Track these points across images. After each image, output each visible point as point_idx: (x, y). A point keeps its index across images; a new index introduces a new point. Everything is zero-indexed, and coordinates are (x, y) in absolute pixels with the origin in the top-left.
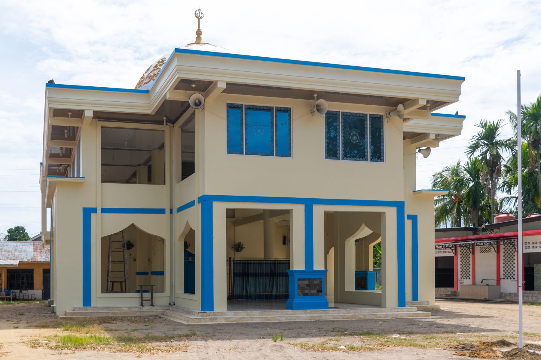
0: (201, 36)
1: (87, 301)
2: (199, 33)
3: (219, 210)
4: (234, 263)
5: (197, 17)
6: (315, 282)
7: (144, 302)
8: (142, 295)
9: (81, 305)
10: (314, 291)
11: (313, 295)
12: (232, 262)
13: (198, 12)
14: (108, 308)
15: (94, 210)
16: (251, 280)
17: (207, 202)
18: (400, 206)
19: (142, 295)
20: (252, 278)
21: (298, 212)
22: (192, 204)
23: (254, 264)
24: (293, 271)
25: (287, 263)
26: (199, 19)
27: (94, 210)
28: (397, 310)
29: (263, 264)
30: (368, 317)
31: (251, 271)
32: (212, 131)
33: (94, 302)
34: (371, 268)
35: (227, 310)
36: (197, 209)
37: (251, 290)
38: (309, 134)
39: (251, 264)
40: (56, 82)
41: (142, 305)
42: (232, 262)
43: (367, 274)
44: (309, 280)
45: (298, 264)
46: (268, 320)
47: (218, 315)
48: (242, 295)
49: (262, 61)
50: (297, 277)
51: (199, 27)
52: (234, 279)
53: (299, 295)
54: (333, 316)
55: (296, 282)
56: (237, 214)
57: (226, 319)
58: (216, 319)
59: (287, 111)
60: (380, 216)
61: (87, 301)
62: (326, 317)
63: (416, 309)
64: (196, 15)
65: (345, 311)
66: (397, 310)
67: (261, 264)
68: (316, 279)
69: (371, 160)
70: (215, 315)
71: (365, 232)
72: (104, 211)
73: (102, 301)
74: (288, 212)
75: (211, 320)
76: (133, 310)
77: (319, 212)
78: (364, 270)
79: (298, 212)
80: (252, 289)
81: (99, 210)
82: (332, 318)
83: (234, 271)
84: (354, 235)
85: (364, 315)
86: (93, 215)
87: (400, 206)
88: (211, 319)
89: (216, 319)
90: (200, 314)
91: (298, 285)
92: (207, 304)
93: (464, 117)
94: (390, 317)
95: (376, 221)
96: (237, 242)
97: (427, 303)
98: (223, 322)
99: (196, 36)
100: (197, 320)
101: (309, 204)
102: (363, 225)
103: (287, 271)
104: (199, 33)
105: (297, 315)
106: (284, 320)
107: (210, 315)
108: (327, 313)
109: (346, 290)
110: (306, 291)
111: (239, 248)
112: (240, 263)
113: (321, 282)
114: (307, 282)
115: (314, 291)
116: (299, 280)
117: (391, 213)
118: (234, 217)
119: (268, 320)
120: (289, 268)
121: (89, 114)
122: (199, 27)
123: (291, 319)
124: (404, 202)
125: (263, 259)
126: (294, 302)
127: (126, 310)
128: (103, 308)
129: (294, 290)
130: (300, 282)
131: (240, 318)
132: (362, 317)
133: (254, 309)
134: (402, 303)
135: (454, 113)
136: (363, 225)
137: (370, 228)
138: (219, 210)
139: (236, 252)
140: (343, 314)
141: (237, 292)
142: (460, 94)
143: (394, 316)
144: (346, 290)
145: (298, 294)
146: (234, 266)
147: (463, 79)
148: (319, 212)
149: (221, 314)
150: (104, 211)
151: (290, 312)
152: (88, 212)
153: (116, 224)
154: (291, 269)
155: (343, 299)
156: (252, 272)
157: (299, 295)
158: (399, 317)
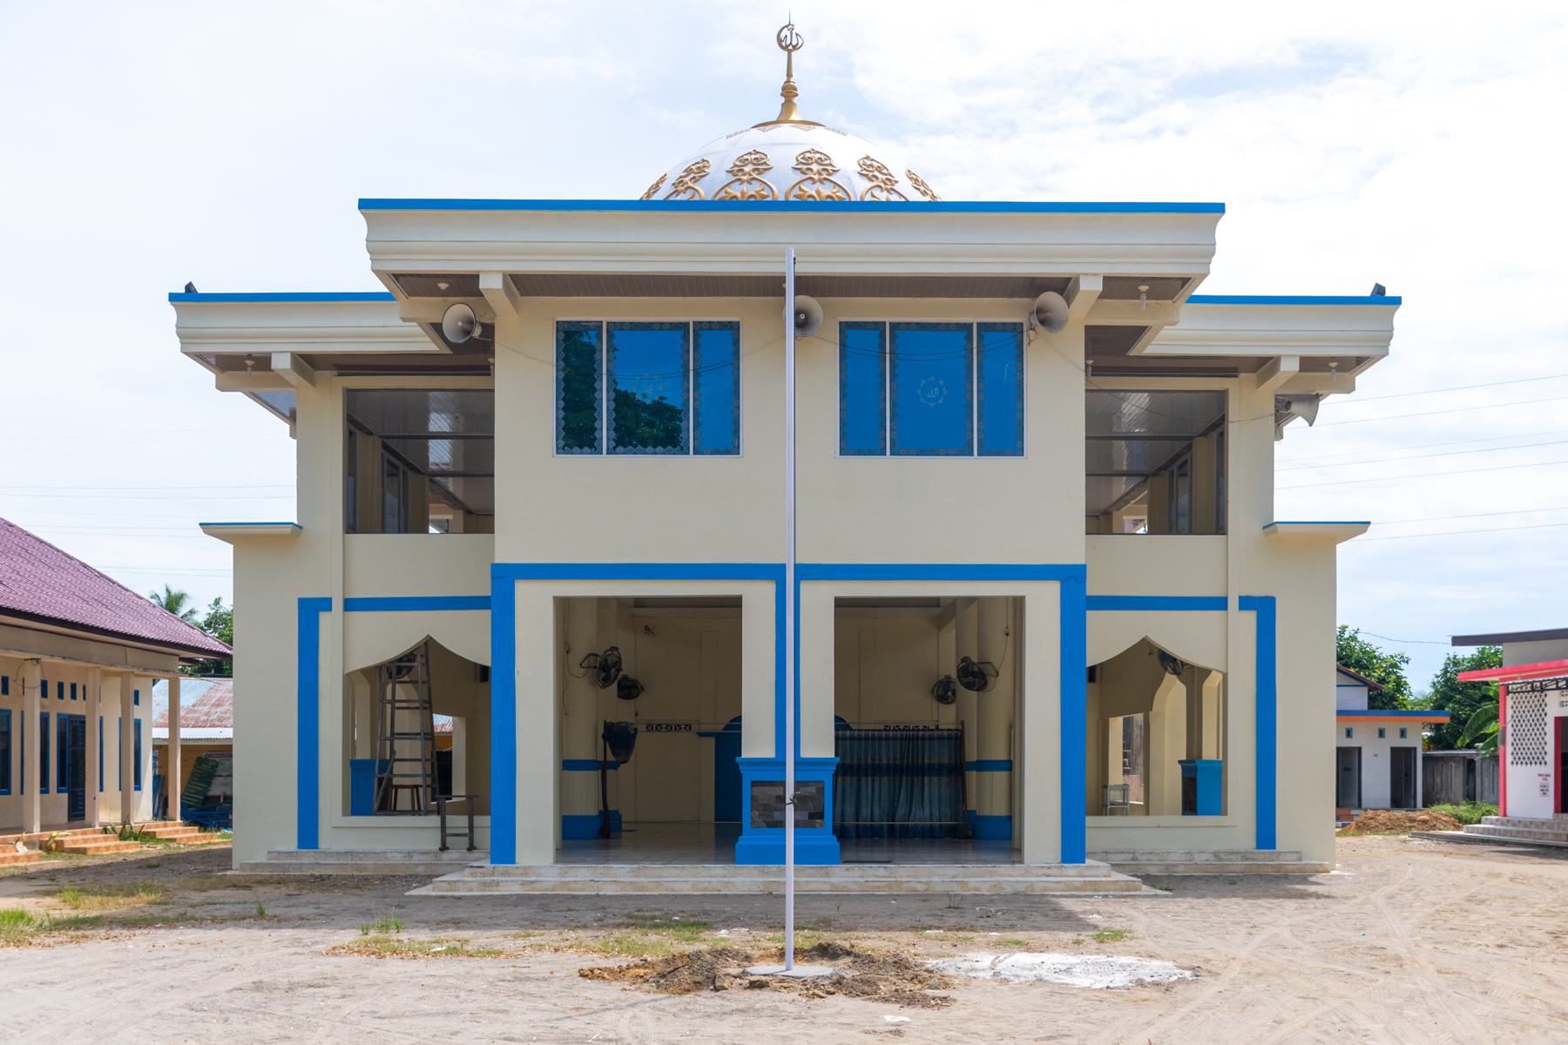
0: (795, 100)
1: (308, 834)
2: (789, 92)
3: (534, 609)
5: (785, 48)
7: (449, 839)
8: (443, 821)
9: (293, 845)
13: (786, 32)
14: (351, 853)
15: (326, 604)
19: (443, 821)
26: (790, 52)
27: (326, 604)
29: (880, 739)
32: (524, 394)
33: (329, 839)
38: (789, 392)
40: (200, 290)
41: (444, 848)
46: (643, 888)
49: (595, 213)
51: (789, 75)
53: (754, 824)
57: (523, 883)
59: (733, 328)
61: (308, 834)
62: (811, 887)
64: (780, 41)
65: (857, 873)
67: (874, 738)
69: (980, 454)
72: (350, 605)
73: (349, 837)
74: (735, 603)
76: (416, 859)
79: (757, 599)
81: (337, 605)
86: (325, 619)
88: (484, 884)
89: (497, 884)
91: (753, 798)
93: (1397, 301)
97: (1295, 856)
98: (517, 890)
99: (783, 100)
104: (789, 92)
108: (827, 875)
116: (754, 784)
121: (281, 363)
122: (789, 75)
127: (398, 859)
128: (339, 854)
130: (758, 791)
133: (924, 862)
135: (1367, 291)
142: (1213, 254)
147: (1219, 208)
148: (818, 600)
150: (350, 605)
152: (311, 610)
153: (385, 638)
157: (754, 824)
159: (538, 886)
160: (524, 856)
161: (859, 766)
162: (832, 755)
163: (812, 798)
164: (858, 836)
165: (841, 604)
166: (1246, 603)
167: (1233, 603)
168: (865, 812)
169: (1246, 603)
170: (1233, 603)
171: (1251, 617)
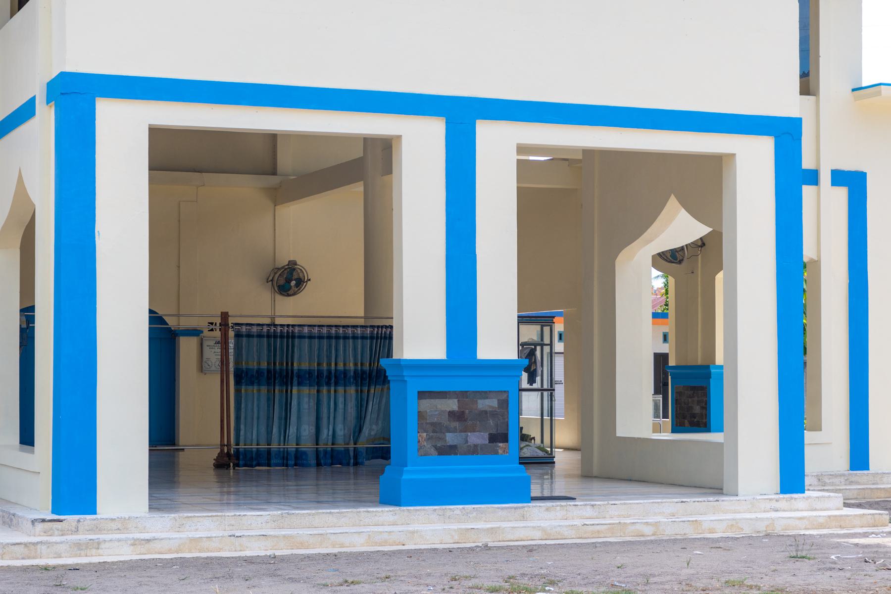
3: (122, 136)
4: (238, 335)
6: (484, 404)
10: (478, 438)
11: (474, 450)
12: (231, 334)
16: (303, 398)
17: (76, 97)
18: (785, 133)
20: (305, 390)
21: (422, 146)
22: (26, 112)
23: (311, 337)
24: (402, 365)
25: (381, 337)
28: (775, 505)
30: (670, 531)
31: (303, 361)
34: (719, 359)
35: (151, 508)
36: (44, 125)
37: (302, 433)
39: (301, 337)
42: (231, 334)
43: (708, 376)
44: (462, 395)
45: (420, 338)
46: (302, 545)
47: (110, 531)
48: (269, 452)
50: (414, 386)
52: (238, 392)
54: (543, 530)
55: (413, 406)
56: (286, 160)
57: (135, 543)
58: (97, 544)
60: (716, 168)
62: (521, 534)
63: (837, 499)
65: (589, 511)
66: (775, 505)
68: (485, 395)
70: (96, 529)
71: (680, 228)
75: (79, 546)
77: (498, 149)
78: (699, 363)
79: (422, 146)
80: (308, 430)
82: (538, 534)
83: (237, 362)
84: (646, 235)
85: (656, 524)
87: (785, 133)
88: (78, 545)
89: (97, 544)
90: (40, 527)
91: (421, 415)
92: (75, 489)
94: (747, 531)
95: (703, 184)
96: (283, 261)
98: (127, 554)
100: (21, 549)
101: (461, 117)
102: (673, 202)
103: (384, 362)
105: (411, 528)
106: (359, 545)
107: (77, 530)
108: (524, 518)
109: (619, 433)
110: (451, 438)
111: (288, 281)
112: (260, 336)
113: (504, 404)
114: (452, 405)
115: (478, 438)
116: (422, 395)
117: (753, 163)
118: (274, 173)
119: (302, 545)
120: (389, 354)
123: (385, 543)
124: (801, 119)
125: (361, 322)
126: (405, 477)
129: (408, 436)
130: (427, 405)
131: (193, 540)
132: (648, 530)
134: (792, 478)
136: (673, 202)
137: (697, 214)
138: (122, 136)
139: (279, 297)
140: (578, 522)
141: (253, 439)
143: (762, 527)
144: (619, 433)
145: (420, 448)
146: (238, 348)
149: (123, 524)
151: (386, 513)
154: (396, 356)
155: (614, 466)
156: (305, 366)
158: (778, 530)
159: (157, 545)
160: (108, 502)
161: (320, 373)
162: (514, 356)
163: (494, 414)
164: (318, 464)
165: (159, 136)
166: (839, 178)
167: (825, 178)
168: (325, 434)
169: (839, 178)
170: (825, 178)
171: (841, 194)
